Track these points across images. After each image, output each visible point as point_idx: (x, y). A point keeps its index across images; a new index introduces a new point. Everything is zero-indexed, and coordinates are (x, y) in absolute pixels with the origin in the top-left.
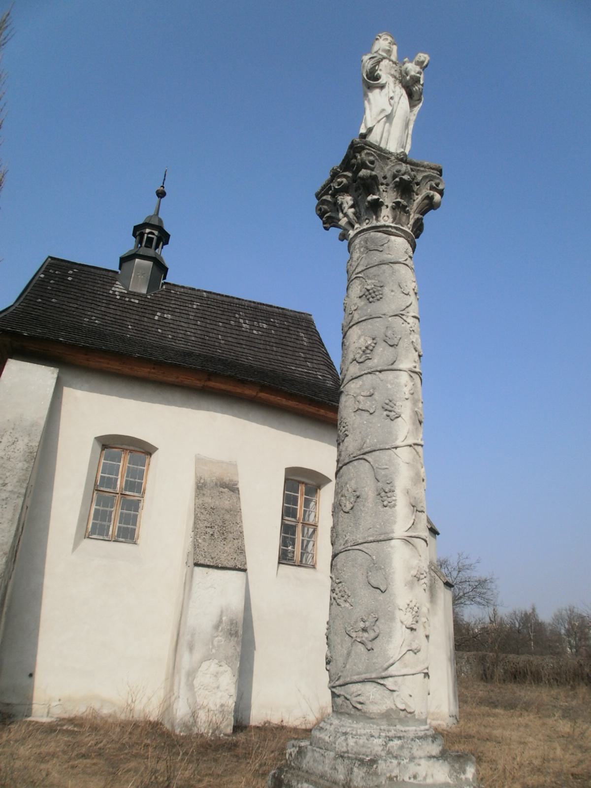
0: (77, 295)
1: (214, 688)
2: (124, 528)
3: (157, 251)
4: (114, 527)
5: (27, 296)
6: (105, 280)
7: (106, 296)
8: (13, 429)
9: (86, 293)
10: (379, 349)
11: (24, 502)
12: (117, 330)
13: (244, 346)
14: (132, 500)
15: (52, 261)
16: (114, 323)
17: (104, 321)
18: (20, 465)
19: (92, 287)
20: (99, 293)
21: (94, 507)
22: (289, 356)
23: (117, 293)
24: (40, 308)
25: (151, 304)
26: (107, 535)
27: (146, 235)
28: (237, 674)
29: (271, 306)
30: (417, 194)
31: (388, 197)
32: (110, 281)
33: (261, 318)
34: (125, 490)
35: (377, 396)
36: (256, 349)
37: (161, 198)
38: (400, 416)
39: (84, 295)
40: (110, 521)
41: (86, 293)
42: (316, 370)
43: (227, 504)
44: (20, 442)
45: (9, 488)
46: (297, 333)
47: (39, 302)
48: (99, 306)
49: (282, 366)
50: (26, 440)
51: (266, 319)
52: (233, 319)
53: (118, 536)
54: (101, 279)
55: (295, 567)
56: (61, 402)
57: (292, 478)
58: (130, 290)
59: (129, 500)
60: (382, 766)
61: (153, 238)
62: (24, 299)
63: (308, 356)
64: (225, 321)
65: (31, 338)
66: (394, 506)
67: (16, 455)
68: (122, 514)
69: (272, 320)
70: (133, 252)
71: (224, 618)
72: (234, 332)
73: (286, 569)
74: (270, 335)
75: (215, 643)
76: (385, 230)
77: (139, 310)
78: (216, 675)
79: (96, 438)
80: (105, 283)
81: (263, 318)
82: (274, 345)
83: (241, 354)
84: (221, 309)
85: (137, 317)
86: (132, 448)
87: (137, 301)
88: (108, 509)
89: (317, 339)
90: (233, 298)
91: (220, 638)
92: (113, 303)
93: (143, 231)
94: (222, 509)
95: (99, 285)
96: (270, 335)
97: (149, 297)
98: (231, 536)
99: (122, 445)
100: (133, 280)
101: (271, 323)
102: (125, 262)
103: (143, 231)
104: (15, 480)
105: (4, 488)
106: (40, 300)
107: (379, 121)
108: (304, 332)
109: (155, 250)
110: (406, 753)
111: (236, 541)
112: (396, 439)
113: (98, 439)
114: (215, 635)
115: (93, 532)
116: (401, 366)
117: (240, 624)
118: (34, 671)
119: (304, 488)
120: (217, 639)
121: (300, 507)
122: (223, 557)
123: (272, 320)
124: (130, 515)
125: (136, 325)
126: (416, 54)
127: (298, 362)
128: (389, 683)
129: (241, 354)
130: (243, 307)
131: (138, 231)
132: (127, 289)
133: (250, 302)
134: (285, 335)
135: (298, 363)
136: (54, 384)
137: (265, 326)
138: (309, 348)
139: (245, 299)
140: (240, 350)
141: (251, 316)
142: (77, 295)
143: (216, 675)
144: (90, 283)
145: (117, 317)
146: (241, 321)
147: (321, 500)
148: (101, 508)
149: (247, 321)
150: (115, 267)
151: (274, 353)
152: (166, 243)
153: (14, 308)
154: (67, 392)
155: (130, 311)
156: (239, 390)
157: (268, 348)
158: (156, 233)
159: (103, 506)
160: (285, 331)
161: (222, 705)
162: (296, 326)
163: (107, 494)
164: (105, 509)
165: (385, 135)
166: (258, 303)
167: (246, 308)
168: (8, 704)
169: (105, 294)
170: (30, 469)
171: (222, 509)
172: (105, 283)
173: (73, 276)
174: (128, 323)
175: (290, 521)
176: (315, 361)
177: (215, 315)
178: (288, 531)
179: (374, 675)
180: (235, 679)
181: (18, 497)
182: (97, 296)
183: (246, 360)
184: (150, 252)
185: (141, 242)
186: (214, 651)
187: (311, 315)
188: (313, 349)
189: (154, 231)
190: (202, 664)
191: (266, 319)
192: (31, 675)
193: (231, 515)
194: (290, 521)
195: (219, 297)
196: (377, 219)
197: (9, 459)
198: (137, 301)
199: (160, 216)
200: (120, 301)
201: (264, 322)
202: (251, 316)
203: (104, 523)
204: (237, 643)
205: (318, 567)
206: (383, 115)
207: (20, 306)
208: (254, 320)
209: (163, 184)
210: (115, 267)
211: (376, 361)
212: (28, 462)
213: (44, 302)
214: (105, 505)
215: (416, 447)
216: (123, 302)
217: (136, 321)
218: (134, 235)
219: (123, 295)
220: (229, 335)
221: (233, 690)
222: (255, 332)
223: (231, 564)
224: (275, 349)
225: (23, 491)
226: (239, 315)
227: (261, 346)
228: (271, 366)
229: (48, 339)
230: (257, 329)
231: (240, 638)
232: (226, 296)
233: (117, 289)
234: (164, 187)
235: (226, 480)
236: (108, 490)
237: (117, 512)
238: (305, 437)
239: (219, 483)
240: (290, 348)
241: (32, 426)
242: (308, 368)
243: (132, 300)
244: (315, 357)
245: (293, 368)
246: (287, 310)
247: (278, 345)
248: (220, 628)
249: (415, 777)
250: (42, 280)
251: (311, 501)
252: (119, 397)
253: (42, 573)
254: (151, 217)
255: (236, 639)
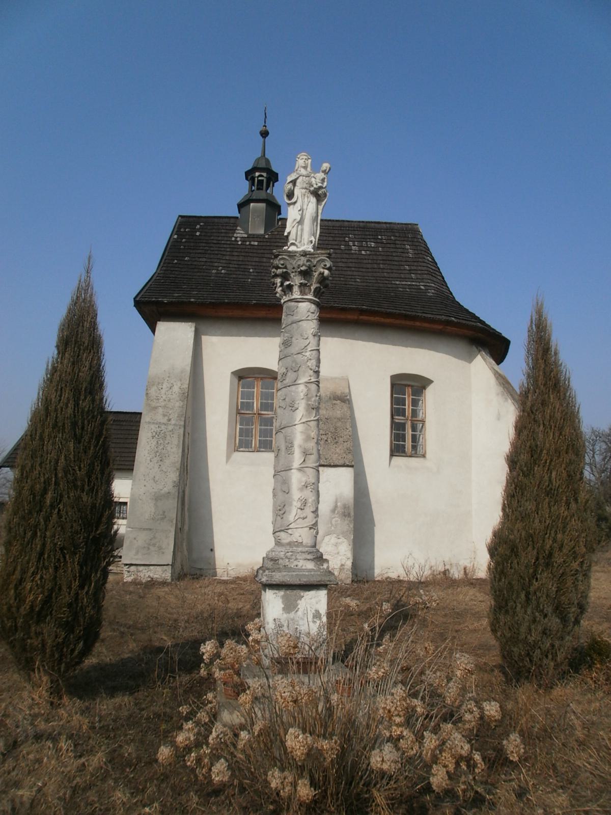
0: (206, 248)
1: (335, 554)
2: (264, 440)
3: (268, 191)
4: (255, 442)
5: (165, 260)
6: (228, 228)
7: (230, 244)
8: (169, 377)
9: (212, 245)
10: (289, 374)
11: (184, 432)
12: (240, 276)
13: (353, 269)
14: (268, 418)
15: (183, 219)
16: (237, 269)
17: (229, 269)
18: (177, 404)
19: (217, 238)
20: (223, 242)
21: (238, 427)
22: (395, 271)
23: (238, 239)
24: (177, 269)
25: (268, 244)
26: (251, 447)
27: (256, 179)
28: (351, 543)
29: (379, 223)
30: (315, 272)
31: (297, 280)
32: (232, 228)
33: (369, 237)
34: (261, 410)
35: (287, 400)
36: (364, 270)
37: (265, 138)
38: (297, 409)
39: (211, 247)
40: (252, 437)
41: (212, 245)
42: (420, 281)
43: (338, 413)
44: (175, 386)
45: (173, 422)
46: (403, 246)
47: (176, 264)
48: (224, 255)
49: (387, 282)
50: (179, 384)
51: (374, 237)
52: (343, 243)
53: (260, 447)
54: (224, 228)
55: (407, 458)
56: (201, 349)
57: (399, 382)
58: (250, 233)
59: (265, 418)
60: (281, 561)
61: (263, 180)
62: (164, 263)
63: (413, 268)
64: (336, 247)
65: (170, 303)
66: (293, 454)
67: (174, 396)
68: (261, 430)
69: (380, 237)
70: (247, 198)
71: (339, 504)
72: (345, 256)
73: (399, 461)
74: (378, 253)
75: (333, 523)
76: (296, 301)
77: (259, 251)
78: (336, 545)
79: (232, 373)
80: (228, 231)
81: (371, 237)
82: (381, 262)
83: (350, 277)
84: (332, 235)
85: (257, 259)
86: (262, 376)
87: (256, 243)
88: (251, 427)
89: (423, 246)
90: (344, 221)
91: (337, 519)
92: (236, 250)
93: (253, 175)
94: (335, 418)
95: (223, 235)
96: (378, 253)
97: (267, 236)
98: (341, 439)
99: (254, 374)
100: (251, 225)
101: (379, 241)
102: (242, 207)
103: (253, 175)
104: (176, 415)
105: (169, 423)
106: (176, 261)
107: (293, 227)
108: (410, 243)
109: (266, 191)
110: (294, 557)
111: (345, 444)
112: (295, 421)
113: (234, 373)
114: (333, 516)
115: (240, 446)
116: (299, 382)
117: (352, 507)
118: (214, 547)
119: (410, 390)
120: (334, 519)
121: (408, 408)
122: (335, 457)
123: (380, 237)
124: (267, 429)
125: (257, 267)
126: (321, 166)
127: (403, 276)
128: (290, 531)
129: (350, 277)
130: (352, 229)
131: (249, 175)
132: (247, 233)
133: (359, 222)
134: (392, 250)
135: (403, 277)
136: (193, 336)
137: (373, 245)
138: (415, 260)
139: (354, 220)
140: (349, 273)
141: (360, 237)
142: (206, 248)
143: (336, 545)
144: (215, 234)
145: (240, 263)
146: (351, 243)
147: (426, 398)
148: (244, 427)
149: (356, 243)
150: (235, 213)
151: (380, 270)
152: (277, 180)
153: (156, 275)
154: (207, 340)
155: (250, 254)
156: (342, 316)
157: (376, 266)
158: (265, 174)
159: (246, 425)
160: (392, 246)
161: (342, 565)
162: (402, 239)
163: (247, 416)
164: (248, 427)
165: (299, 233)
166: (367, 222)
167: (355, 229)
168: (201, 569)
169: (229, 242)
170: (185, 406)
171: (335, 418)
172: (228, 231)
173: (201, 230)
174: (250, 267)
175: (399, 419)
176: (419, 272)
177: (327, 242)
178: (397, 429)
179: (283, 529)
180: (350, 547)
181: (180, 428)
182: (222, 246)
183: (354, 283)
184: (262, 195)
185: (253, 184)
186: (333, 528)
187: (417, 225)
188: (417, 260)
189: (263, 174)
190: (325, 538)
191: (374, 237)
192: (212, 550)
193: (342, 422)
194: (399, 419)
195: (330, 222)
196: (292, 295)
197: (169, 400)
198: (256, 243)
199: (266, 156)
200: (242, 246)
201: (372, 240)
202: (360, 237)
203: (248, 438)
204: (350, 521)
205: (428, 456)
206: (295, 223)
207: (161, 272)
208: (363, 240)
209: (265, 122)
210: (235, 213)
211: (288, 381)
212: (182, 401)
213: (180, 262)
214: (247, 424)
215: (308, 423)
216: (244, 247)
217: (257, 264)
218: (247, 179)
219: (244, 240)
220: (339, 260)
221: (349, 555)
222: (363, 252)
223: (341, 462)
224: (381, 266)
225: (182, 423)
226: (349, 237)
227: (369, 266)
228: (377, 285)
229: (182, 303)
230: (365, 249)
231: (352, 518)
232: (337, 221)
233: (238, 235)
234: (266, 126)
235: (339, 393)
236: (248, 412)
237: (256, 428)
238: (407, 347)
239: (332, 397)
240: (396, 263)
241: (182, 372)
242: (412, 280)
243: (252, 243)
244: (420, 268)
245: (397, 283)
246: (395, 224)
247: (385, 262)
248: (336, 512)
249: (297, 566)
250: (176, 241)
251: (419, 400)
252: (247, 336)
253: (207, 480)
254: (258, 160)
255: (349, 519)
